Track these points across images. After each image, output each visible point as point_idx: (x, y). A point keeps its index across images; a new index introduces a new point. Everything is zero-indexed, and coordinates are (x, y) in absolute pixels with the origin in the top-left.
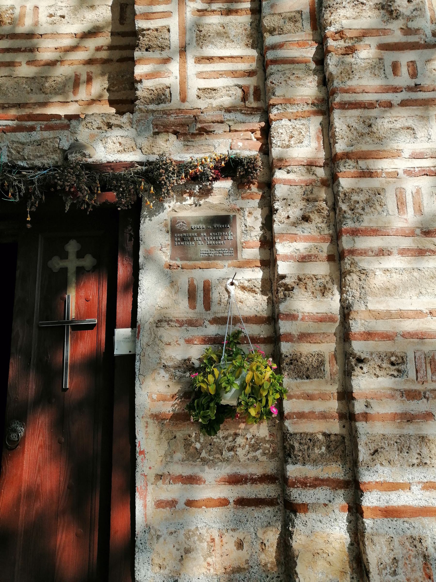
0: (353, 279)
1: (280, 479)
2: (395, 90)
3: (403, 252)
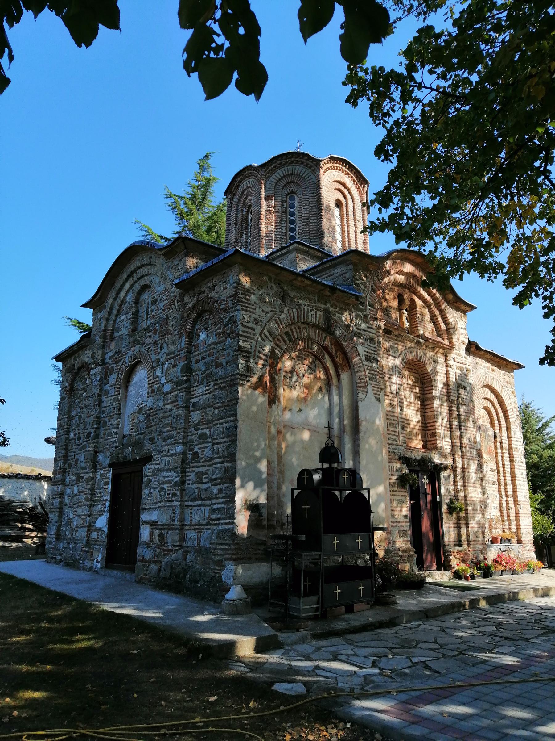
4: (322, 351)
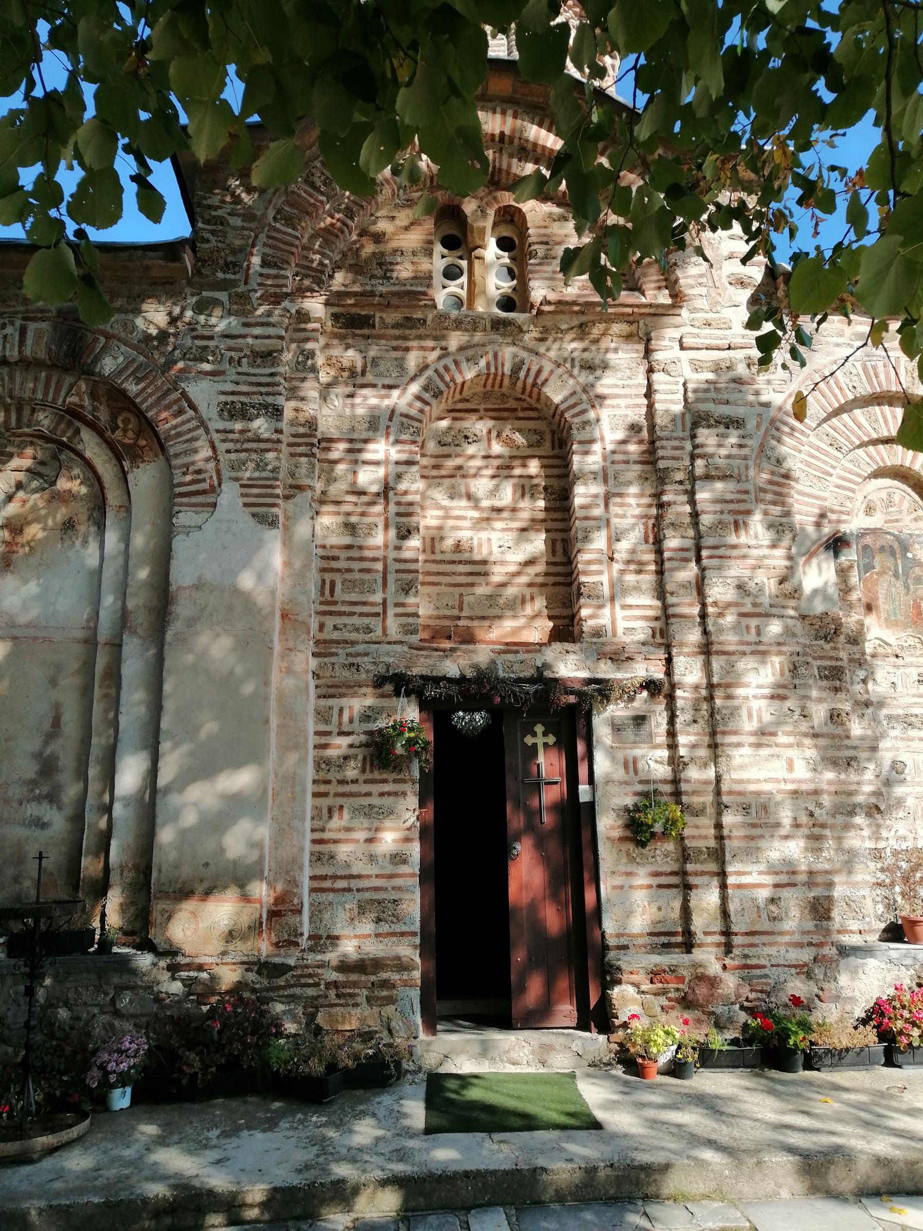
0: (722, 760)
1: (683, 873)
2: (748, 644)
3: (751, 745)
4: (70, 424)
